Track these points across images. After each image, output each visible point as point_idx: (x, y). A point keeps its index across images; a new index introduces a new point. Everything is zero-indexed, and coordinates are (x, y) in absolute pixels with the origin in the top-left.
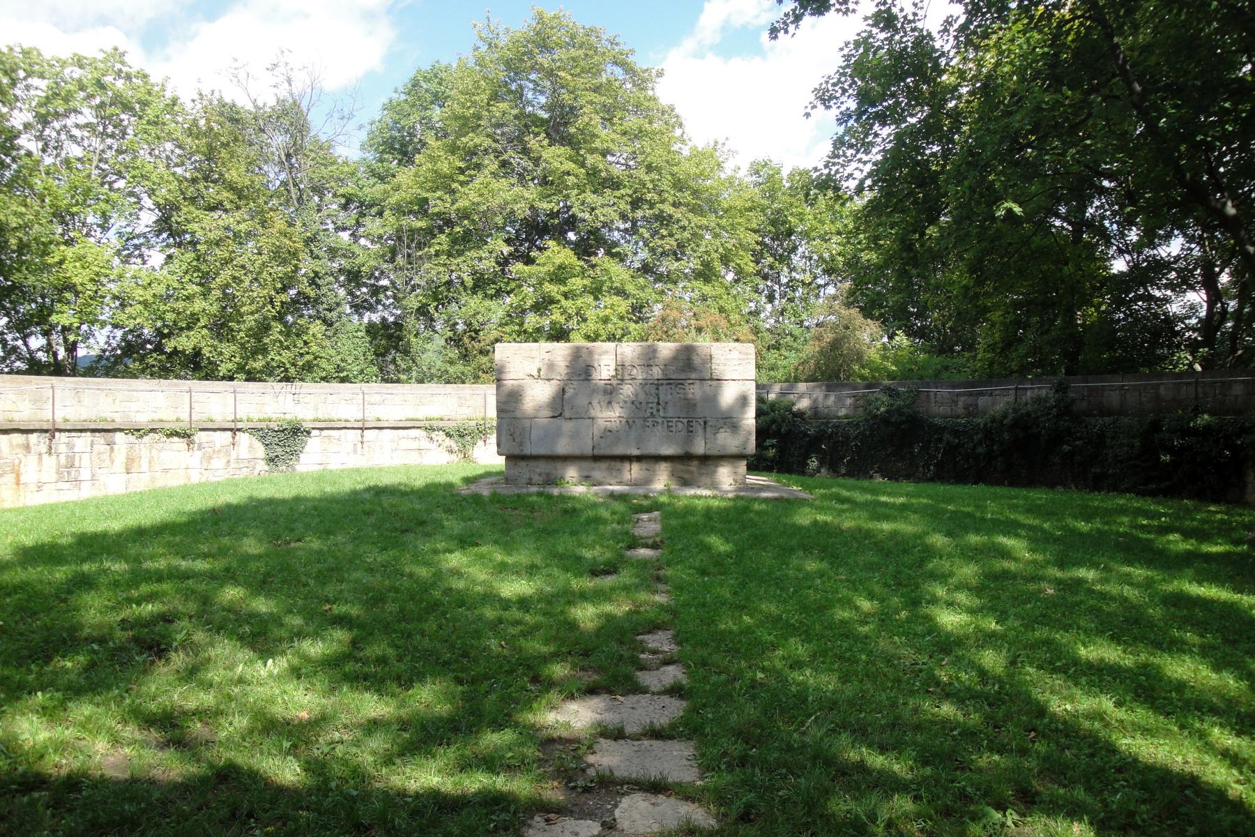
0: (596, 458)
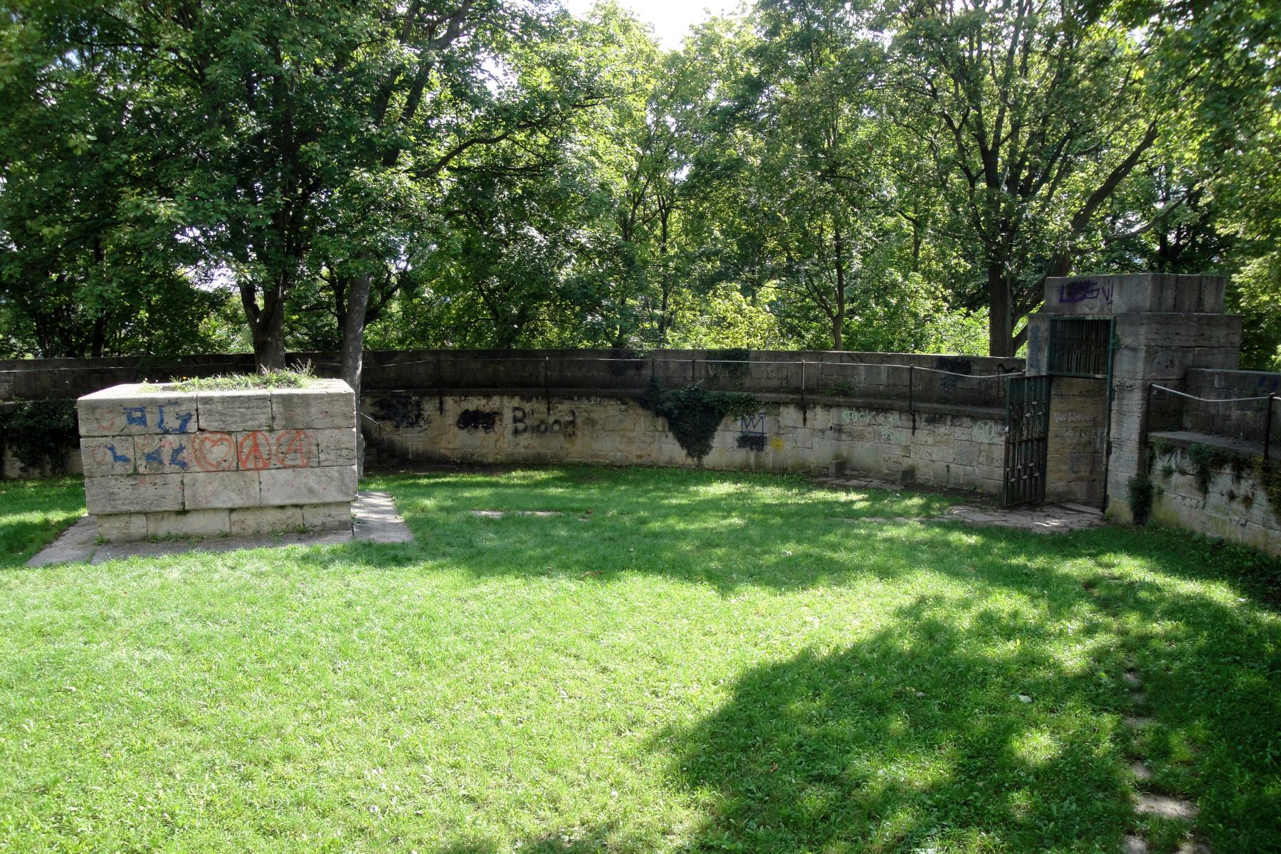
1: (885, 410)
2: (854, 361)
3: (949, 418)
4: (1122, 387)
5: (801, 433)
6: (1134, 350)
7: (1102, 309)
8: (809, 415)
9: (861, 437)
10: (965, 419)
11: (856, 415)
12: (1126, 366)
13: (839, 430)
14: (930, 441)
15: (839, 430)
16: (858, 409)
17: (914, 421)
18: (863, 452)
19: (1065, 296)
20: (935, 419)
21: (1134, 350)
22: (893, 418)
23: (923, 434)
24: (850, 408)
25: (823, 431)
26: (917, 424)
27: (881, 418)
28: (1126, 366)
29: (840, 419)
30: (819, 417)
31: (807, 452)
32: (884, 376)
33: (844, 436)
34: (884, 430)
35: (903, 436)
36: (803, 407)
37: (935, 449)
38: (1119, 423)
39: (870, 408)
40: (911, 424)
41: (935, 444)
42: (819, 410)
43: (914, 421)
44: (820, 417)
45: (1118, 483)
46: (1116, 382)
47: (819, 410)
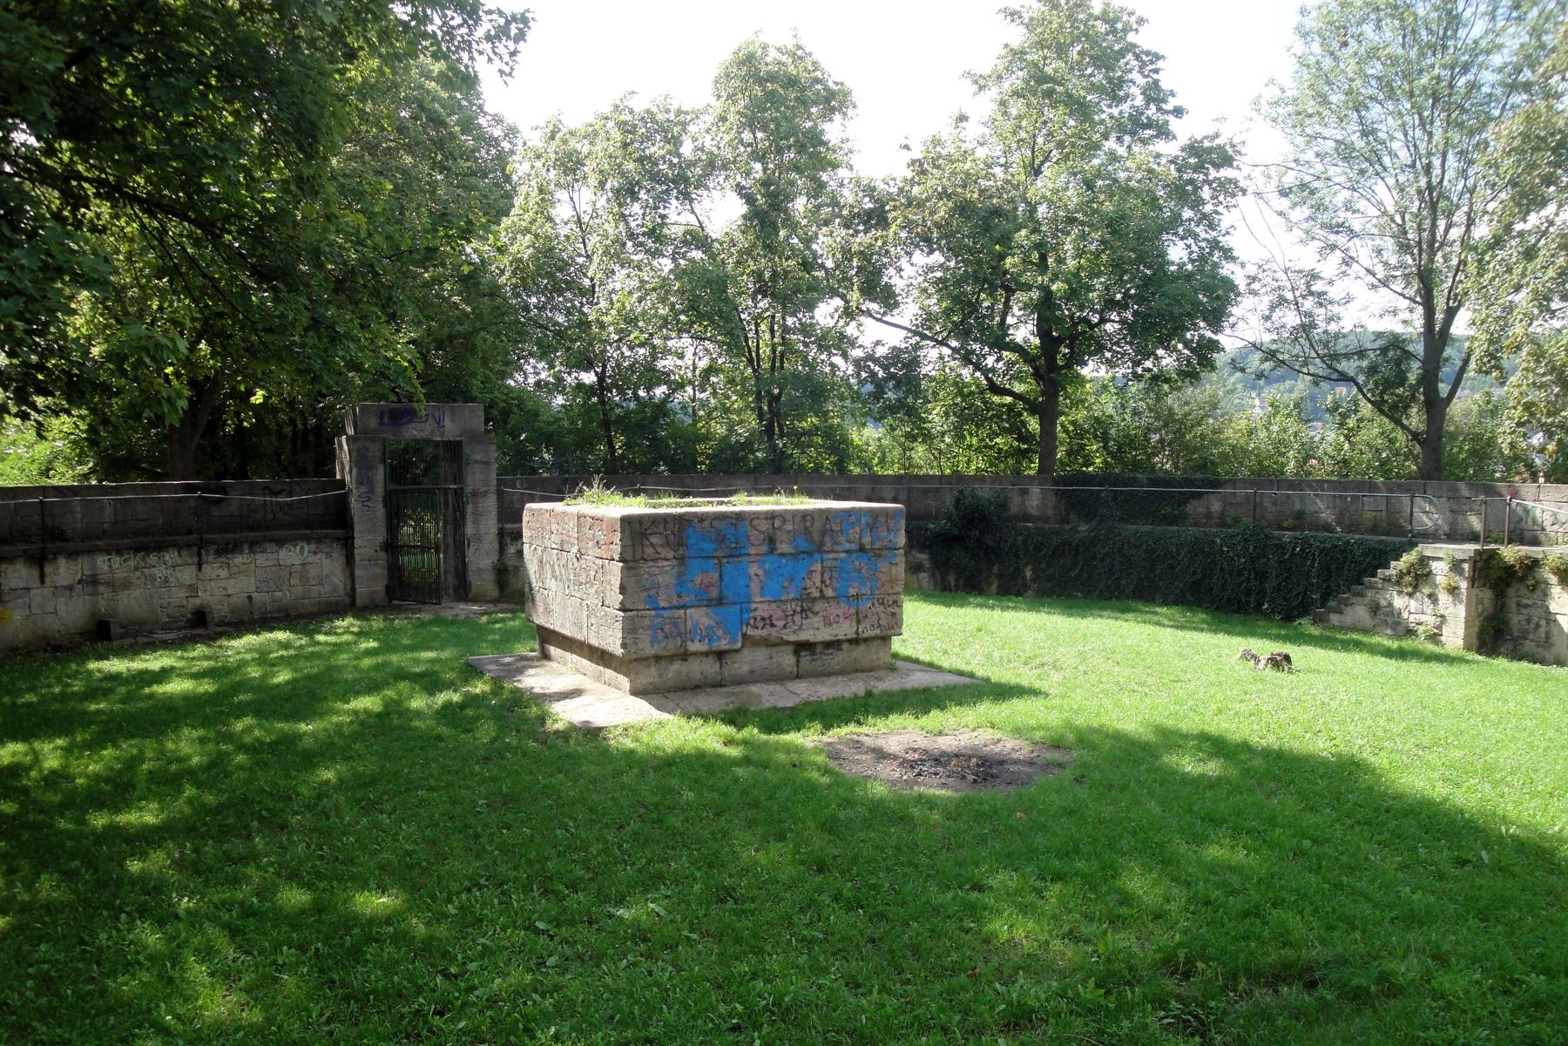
0: (775, 645)
1: (160, 548)
2: (65, 495)
3: (246, 546)
4: (475, 494)
5: (37, 594)
6: (486, 463)
7: (432, 432)
8: (48, 569)
9: (127, 585)
10: (267, 545)
11: (116, 560)
12: (478, 476)
13: (93, 581)
14: (224, 573)
15: (93, 581)
16: (119, 552)
17: (199, 555)
18: (131, 603)
19: (386, 420)
20: (226, 550)
21: (486, 463)
22: (170, 556)
23: (213, 569)
24: (108, 552)
25: (70, 588)
26: (204, 558)
27: (153, 559)
28: (478, 476)
29: (94, 567)
30: (62, 570)
31: (50, 618)
32: (108, 511)
33: (101, 589)
34: (159, 572)
35: (187, 575)
36: (39, 560)
37: (232, 582)
38: (476, 522)
39: (136, 549)
40: (196, 559)
41: (231, 576)
42: (62, 562)
43: (199, 555)
44: (64, 571)
45: (480, 570)
46: (468, 489)
47: (62, 562)
